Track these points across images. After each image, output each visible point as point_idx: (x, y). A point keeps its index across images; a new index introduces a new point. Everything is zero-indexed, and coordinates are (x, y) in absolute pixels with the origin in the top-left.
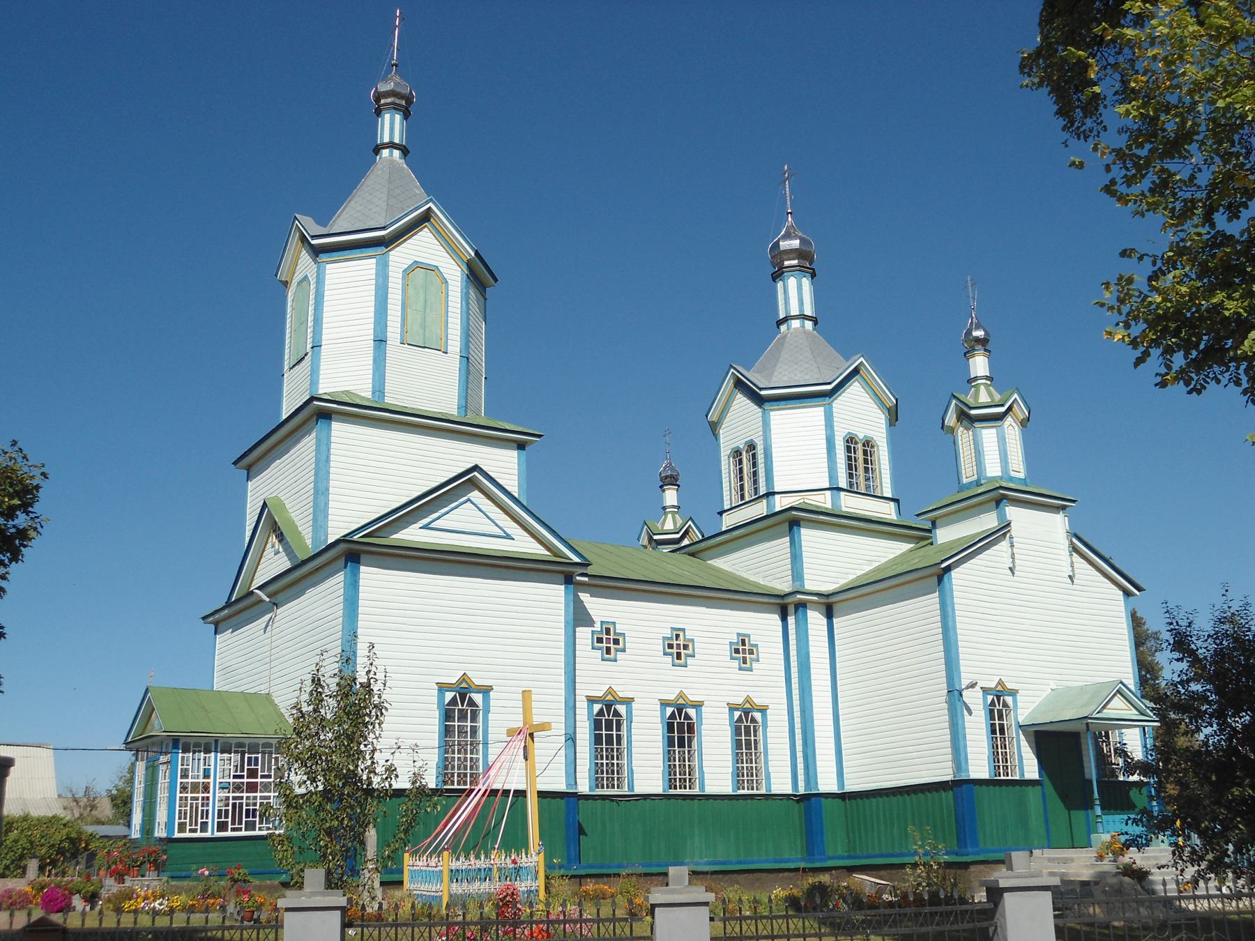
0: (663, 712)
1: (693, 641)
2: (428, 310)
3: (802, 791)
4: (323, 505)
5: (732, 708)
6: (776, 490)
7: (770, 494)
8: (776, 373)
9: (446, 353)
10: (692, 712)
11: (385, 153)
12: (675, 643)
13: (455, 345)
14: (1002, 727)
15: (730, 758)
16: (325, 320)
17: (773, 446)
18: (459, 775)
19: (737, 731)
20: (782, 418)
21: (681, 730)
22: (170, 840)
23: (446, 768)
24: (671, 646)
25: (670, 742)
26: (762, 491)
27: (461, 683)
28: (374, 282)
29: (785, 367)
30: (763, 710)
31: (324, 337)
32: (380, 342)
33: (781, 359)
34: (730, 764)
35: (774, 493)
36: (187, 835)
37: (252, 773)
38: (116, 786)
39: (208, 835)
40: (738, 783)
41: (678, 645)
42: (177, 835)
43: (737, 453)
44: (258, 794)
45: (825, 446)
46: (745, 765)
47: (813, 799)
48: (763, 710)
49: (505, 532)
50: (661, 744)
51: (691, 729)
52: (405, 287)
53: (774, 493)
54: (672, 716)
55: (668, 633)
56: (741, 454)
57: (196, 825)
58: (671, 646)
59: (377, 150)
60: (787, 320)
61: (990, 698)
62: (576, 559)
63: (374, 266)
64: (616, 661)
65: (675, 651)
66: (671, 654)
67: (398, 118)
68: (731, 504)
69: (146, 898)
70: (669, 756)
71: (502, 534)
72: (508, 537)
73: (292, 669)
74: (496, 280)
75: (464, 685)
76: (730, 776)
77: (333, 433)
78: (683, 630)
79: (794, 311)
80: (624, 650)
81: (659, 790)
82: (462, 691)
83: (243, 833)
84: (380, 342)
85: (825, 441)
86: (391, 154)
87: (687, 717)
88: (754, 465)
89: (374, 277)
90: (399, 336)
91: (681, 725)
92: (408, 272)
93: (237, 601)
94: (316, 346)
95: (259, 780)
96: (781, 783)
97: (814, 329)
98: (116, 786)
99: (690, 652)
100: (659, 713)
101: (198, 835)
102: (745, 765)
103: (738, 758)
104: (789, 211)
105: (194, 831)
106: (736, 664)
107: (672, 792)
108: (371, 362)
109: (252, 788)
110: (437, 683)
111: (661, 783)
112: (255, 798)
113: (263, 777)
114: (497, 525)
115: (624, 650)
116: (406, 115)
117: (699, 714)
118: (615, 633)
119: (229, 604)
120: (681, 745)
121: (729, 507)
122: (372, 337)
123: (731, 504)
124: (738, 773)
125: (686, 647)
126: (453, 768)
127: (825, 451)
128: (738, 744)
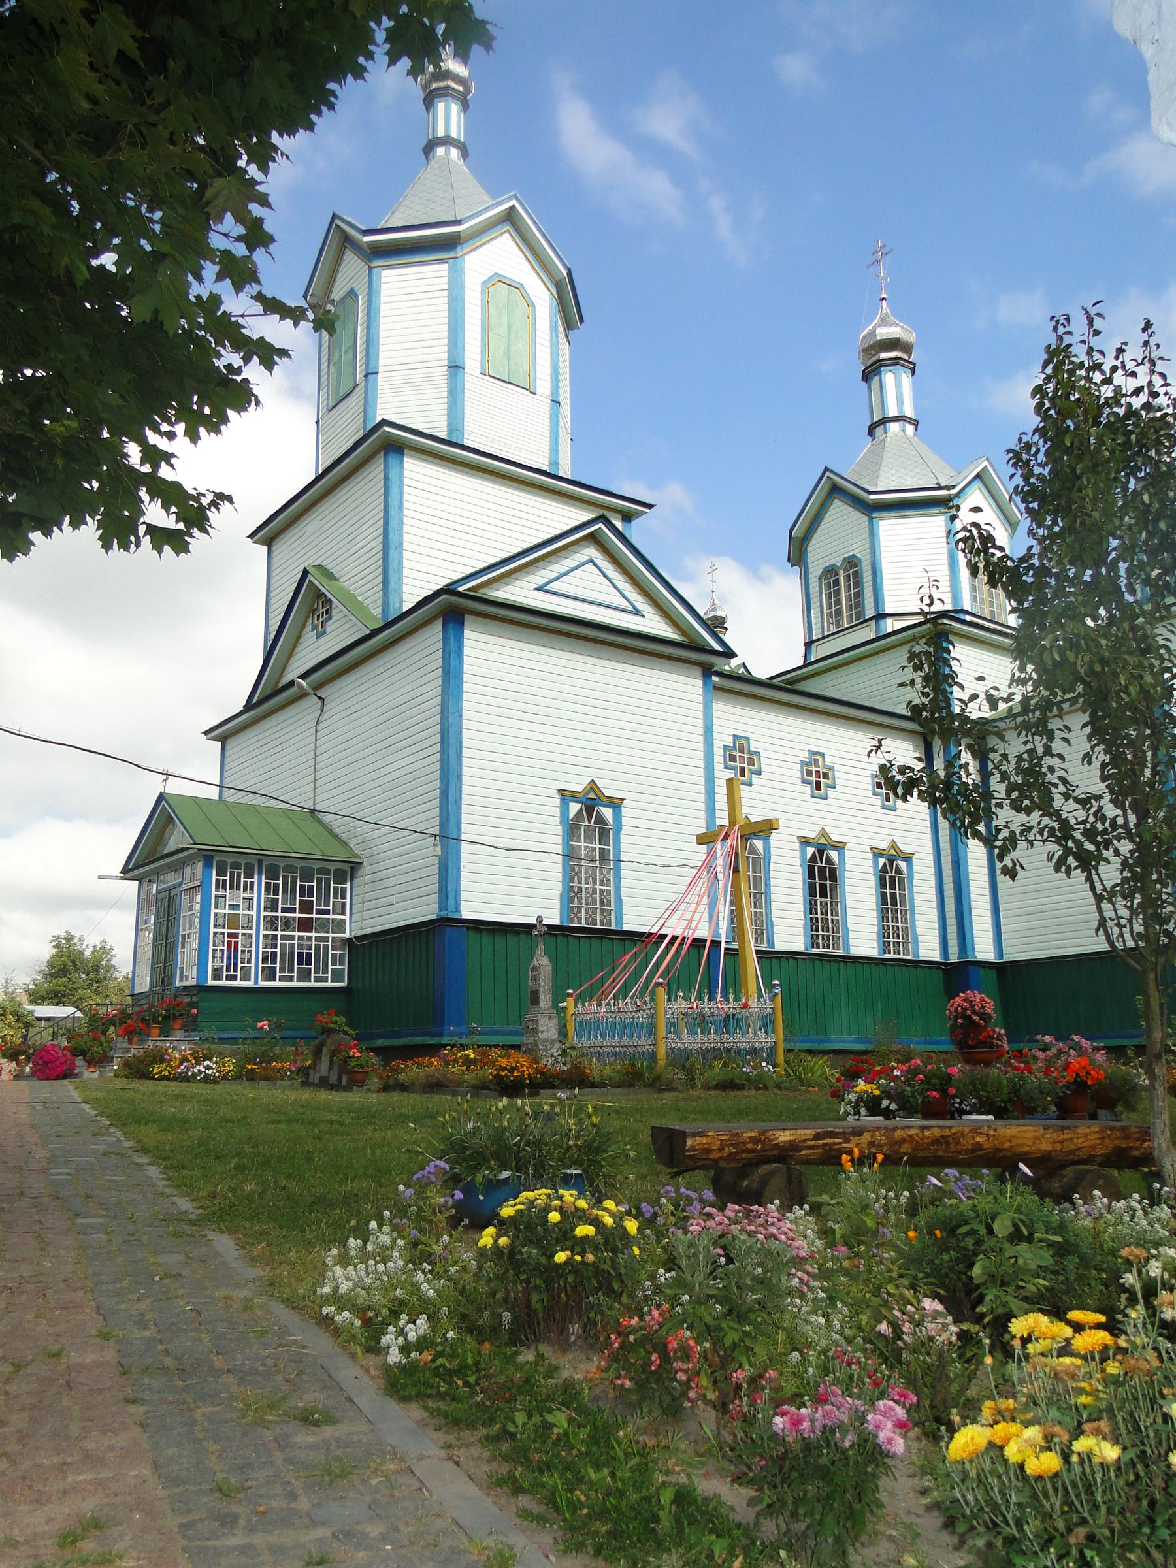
0: (803, 853)
1: (832, 768)
2: (512, 336)
3: (954, 958)
4: (396, 562)
5: (876, 853)
6: (888, 611)
7: (880, 616)
8: (881, 478)
9: (534, 393)
10: (834, 855)
11: (440, 151)
12: (814, 769)
13: (544, 386)
14: (893, 896)
15: (875, 914)
16: (381, 341)
17: (883, 560)
18: (587, 910)
19: (882, 881)
20: (890, 529)
21: (822, 877)
22: (202, 989)
23: (571, 900)
24: (809, 773)
25: (812, 892)
26: (870, 612)
27: (588, 793)
28: (446, 293)
29: (893, 472)
30: (908, 858)
31: (381, 362)
32: (456, 368)
33: (884, 463)
34: (875, 922)
35: (886, 616)
36: (224, 983)
37: (306, 907)
38: (34, 980)
39: (251, 984)
40: (885, 947)
41: (817, 772)
42: (211, 982)
43: (830, 573)
44: (313, 934)
45: (946, 562)
46: (890, 924)
47: (971, 968)
48: (908, 858)
49: (634, 607)
50: (801, 892)
51: (833, 872)
52: (485, 303)
53: (886, 616)
54: (813, 859)
55: (805, 756)
56: (837, 574)
57: (235, 970)
58: (809, 773)
59: (429, 148)
60: (884, 423)
61: (881, 861)
62: (717, 647)
63: (446, 273)
64: (751, 785)
65: (814, 779)
66: (810, 783)
67: (455, 108)
68: (823, 632)
69: (184, 1059)
70: (811, 907)
71: (629, 608)
72: (637, 612)
73: (350, 777)
74: (582, 321)
75: (592, 795)
76: (875, 936)
77: (406, 473)
78: (822, 754)
79: (892, 412)
80: (759, 773)
81: (801, 948)
82: (590, 803)
83: (295, 984)
84: (456, 368)
85: (946, 556)
86: (448, 153)
87: (829, 861)
88: (858, 583)
89: (446, 287)
90: (478, 365)
91: (822, 870)
92: (486, 286)
93: (261, 702)
94: (370, 374)
95: (314, 916)
96: (929, 950)
97: (915, 435)
98: (34, 980)
99: (829, 782)
100: (798, 854)
101: (238, 983)
102: (890, 924)
103: (883, 915)
104: (883, 296)
105: (234, 978)
106: (878, 801)
107: (815, 950)
108: (446, 394)
109: (306, 925)
110: (559, 790)
111: (802, 939)
112: (310, 938)
113: (319, 912)
114: (624, 597)
115: (759, 773)
116: (465, 105)
117: (842, 857)
118: (750, 752)
119: (249, 707)
120: (823, 895)
121: (820, 636)
122: (446, 362)
123: (823, 632)
124: (884, 933)
125: (826, 776)
126: (580, 902)
127: (946, 567)
128: (883, 897)
